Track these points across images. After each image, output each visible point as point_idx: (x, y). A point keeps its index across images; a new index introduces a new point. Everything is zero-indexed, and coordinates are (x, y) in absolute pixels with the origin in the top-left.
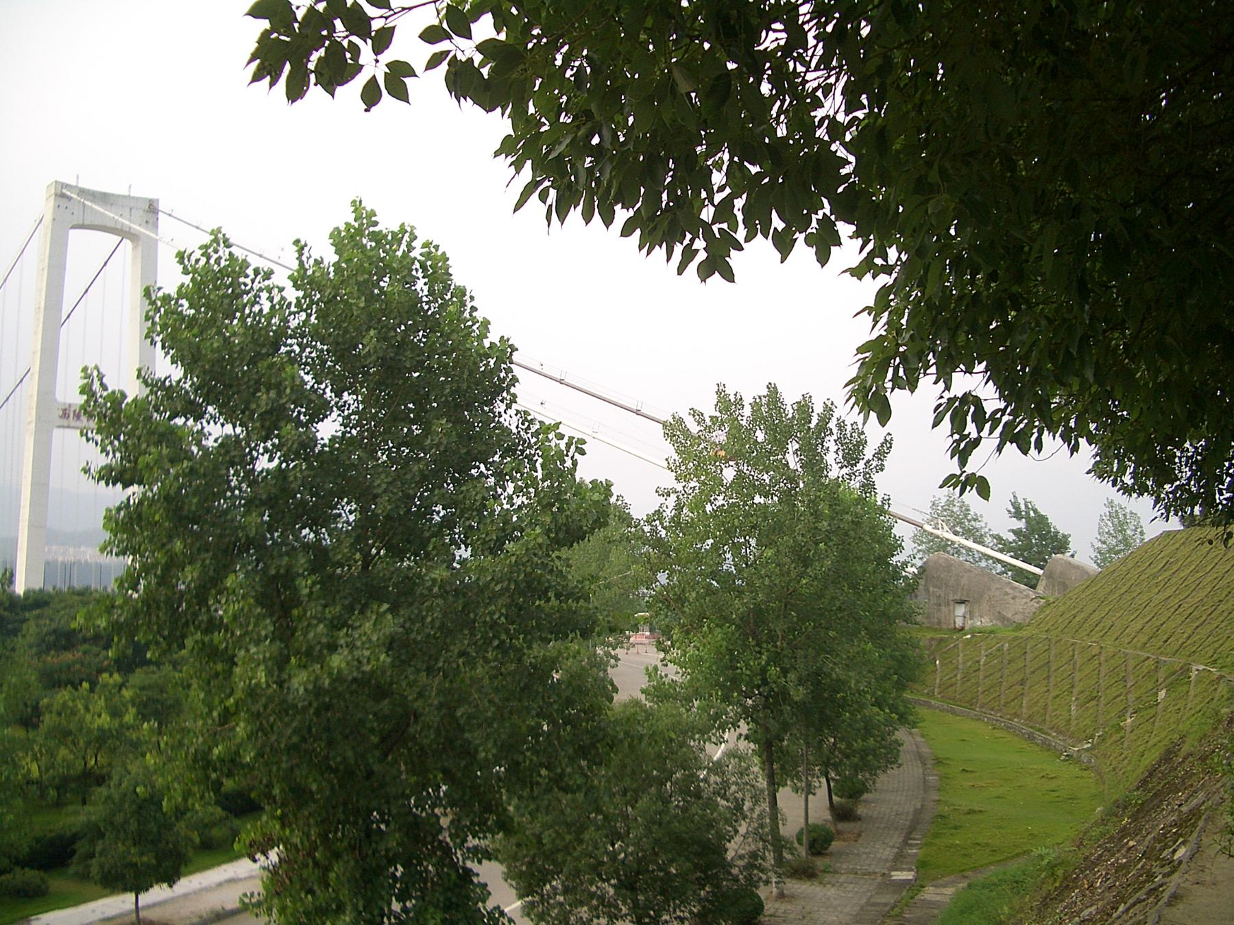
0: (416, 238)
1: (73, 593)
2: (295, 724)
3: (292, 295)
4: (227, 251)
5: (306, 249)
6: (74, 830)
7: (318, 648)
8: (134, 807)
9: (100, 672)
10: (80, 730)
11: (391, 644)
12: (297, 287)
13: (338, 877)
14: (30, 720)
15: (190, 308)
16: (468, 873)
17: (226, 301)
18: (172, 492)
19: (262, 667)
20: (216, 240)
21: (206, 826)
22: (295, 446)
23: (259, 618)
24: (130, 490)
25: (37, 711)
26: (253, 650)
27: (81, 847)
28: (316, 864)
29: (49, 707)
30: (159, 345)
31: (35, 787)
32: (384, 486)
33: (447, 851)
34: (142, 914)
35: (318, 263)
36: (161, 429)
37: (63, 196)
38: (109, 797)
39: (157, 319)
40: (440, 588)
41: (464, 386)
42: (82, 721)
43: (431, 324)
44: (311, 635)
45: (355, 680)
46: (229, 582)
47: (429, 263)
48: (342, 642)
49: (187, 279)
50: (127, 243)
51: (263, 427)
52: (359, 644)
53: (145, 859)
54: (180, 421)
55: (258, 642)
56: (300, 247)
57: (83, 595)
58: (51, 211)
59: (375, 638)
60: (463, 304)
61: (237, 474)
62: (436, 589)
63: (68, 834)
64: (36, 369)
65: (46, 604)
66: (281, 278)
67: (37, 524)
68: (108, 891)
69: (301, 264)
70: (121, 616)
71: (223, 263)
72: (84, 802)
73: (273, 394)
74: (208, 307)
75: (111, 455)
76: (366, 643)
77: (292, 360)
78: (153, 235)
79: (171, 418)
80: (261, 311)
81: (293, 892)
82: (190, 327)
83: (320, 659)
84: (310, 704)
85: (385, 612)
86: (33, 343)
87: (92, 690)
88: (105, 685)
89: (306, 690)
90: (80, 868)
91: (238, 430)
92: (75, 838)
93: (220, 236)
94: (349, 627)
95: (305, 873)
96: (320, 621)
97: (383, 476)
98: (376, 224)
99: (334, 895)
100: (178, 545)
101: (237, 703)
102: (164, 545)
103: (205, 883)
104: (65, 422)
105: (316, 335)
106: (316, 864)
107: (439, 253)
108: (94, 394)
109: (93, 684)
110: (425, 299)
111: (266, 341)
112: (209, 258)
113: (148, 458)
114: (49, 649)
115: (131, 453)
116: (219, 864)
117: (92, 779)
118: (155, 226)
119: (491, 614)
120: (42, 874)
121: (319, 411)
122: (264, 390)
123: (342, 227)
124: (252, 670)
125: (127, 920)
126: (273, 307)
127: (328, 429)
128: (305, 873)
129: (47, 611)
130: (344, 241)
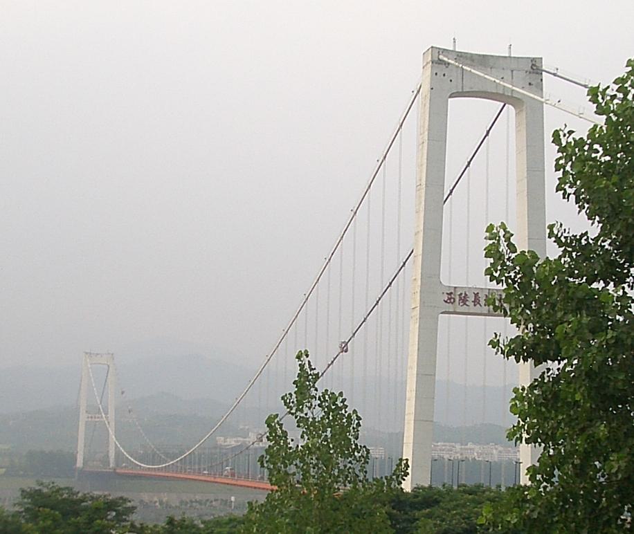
1: (464, 492)
15: (605, 155)
18: (595, 368)
30: (572, 197)
36: (580, 294)
37: (440, 62)
39: (568, 168)
50: (510, 109)
54: (599, 285)
57: (475, 493)
58: (429, 79)
64: (419, 251)
65: (437, 502)
67: (422, 419)
75: (522, 327)
78: (539, 98)
79: (590, 282)
82: (606, 175)
86: (414, 222)
102: (583, 430)
104: (450, 308)
108: (501, 255)
115: (546, 324)
129: (437, 511)
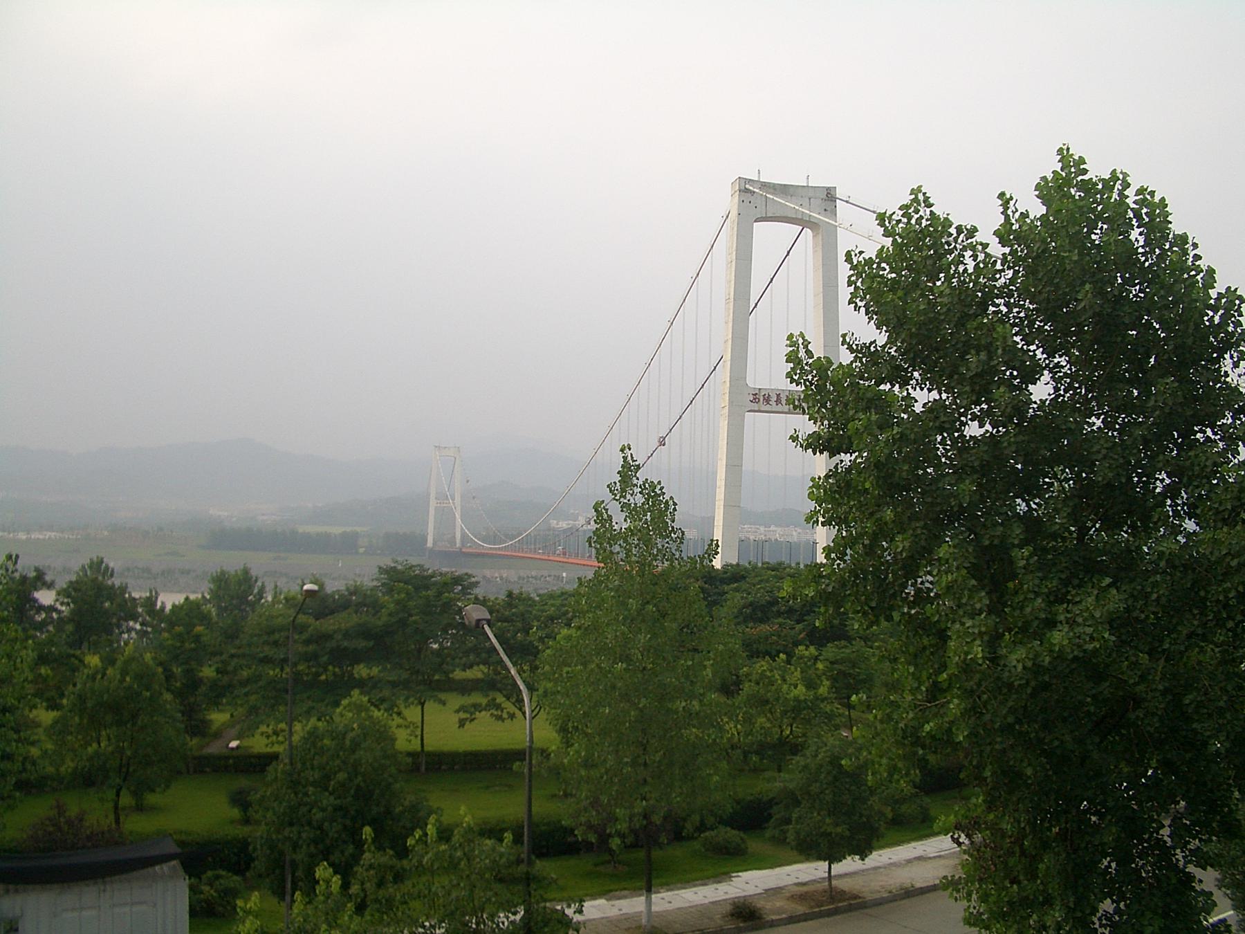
0: (1129, 185)
1: (768, 568)
2: (1010, 704)
3: (997, 250)
4: (928, 210)
5: (1012, 203)
6: (771, 795)
7: (1036, 623)
8: (830, 778)
9: (796, 644)
10: (777, 700)
11: (1113, 622)
12: (1003, 242)
13: (1048, 868)
14: (729, 688)
15: (891, 272)
16: (1190, 878)
17: (929, 262)
19: (978, 642)
20: (916, 200)
21: (897, 802)
22: (1009, 410)
23: (972, 590)
24: (836, 459)
25: (738, 683)
26: (969, 623)
27: (778, 812)
28: (1023, 853)
29: (747, 675)
30: (863, 310)
31: (739, 751)
32: (1104, 452)
33: (1165, 853)
34: (834, 882)
35: (1024, 215)
36: (869, 395)
38: (806, 767)
39: (859, 284)
40: (1167, 561)
41: (1190, 341)
42: (778, 691)
43: (1150, 277)
44: (1028, 610)
45: (1076, 658)
46: (943, 552)
47: (1145, 210)
48: (1062, 618)
49: (888, 242)
50: (807, 231)
51: (973, 391)
52: (1080, 620)
53: (839, 830)
55: (973, 615)
56: (1005, 201)
59: (1097, 614)
60: (1185, 253)
61: (943, 442)
62: (1162, 564)
63: (765, 799)
64: (728, 357)
65: (744, 577)
66: (986, 235)
67: (732, 504)
68: (802, 858)
69: (1007, 217)
70: (827, 586)
71: (924, 223)
72: (780, 771)
73: (983, 356)
74: (908, 268)
76: (1085, 621)
77: (1002, 319)
79: (878, 384)
80: (965, 270)
81: (997, 881)
82: (893, 290)
83: (1040, 637)
84: (1027, 683)
85: (1109, 586)
87: (788, 662)
88: (801, 658)
89: (1024, 668)
90: (777, 833)
91: (944, 396)
92: (771, 802)
93: (921, 197)
94: (1069, 602)
95: (1012, 861)
96: (1037, 594)
97: (1102, 442)
98: (1085, 172)
99: (1041, 888)
100: (889, 514)
101: (950, 677)
102: (872, 514)
103: (895, 859)
105: (1024, 293)
106: (1023, 853)
107: (1157, 199)
108: (801, 361)
109: (790, 655)
110: (1141, 250)
111: (971, 301)
112: (910, 219)
113: (858, 424)
114: (745, 621)
115: (839, 421)
116: (909, 841)
117: (786, 749)
118: (833, 213)
119: (1226, 591)
120: (742, 835)
121: (1031, 376)
122: (973, 352)
123: (1050, 176)
124: (966, 645)
125: (819, 887)
126: (977, 266)
127: (1041, 390)
128: (1012, 861)
129: (744, 585)
130: (1050, 191)
